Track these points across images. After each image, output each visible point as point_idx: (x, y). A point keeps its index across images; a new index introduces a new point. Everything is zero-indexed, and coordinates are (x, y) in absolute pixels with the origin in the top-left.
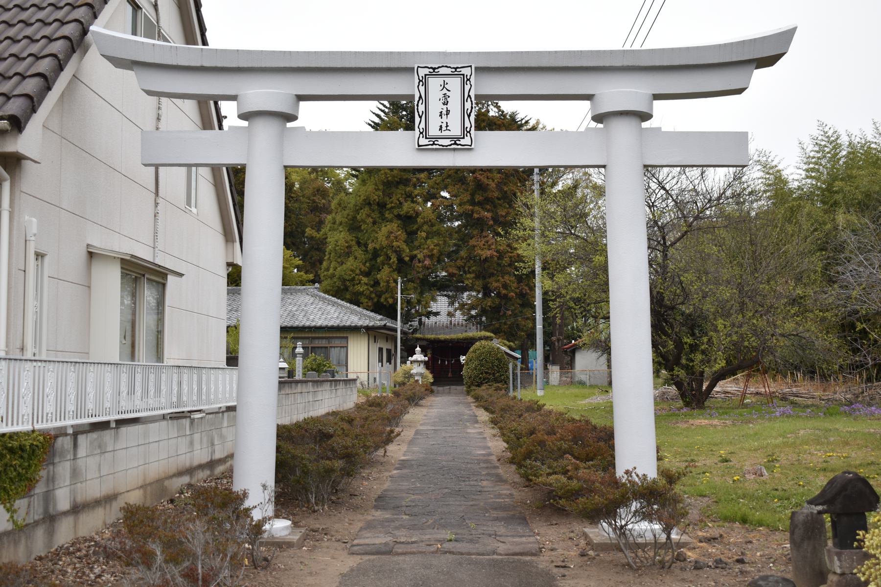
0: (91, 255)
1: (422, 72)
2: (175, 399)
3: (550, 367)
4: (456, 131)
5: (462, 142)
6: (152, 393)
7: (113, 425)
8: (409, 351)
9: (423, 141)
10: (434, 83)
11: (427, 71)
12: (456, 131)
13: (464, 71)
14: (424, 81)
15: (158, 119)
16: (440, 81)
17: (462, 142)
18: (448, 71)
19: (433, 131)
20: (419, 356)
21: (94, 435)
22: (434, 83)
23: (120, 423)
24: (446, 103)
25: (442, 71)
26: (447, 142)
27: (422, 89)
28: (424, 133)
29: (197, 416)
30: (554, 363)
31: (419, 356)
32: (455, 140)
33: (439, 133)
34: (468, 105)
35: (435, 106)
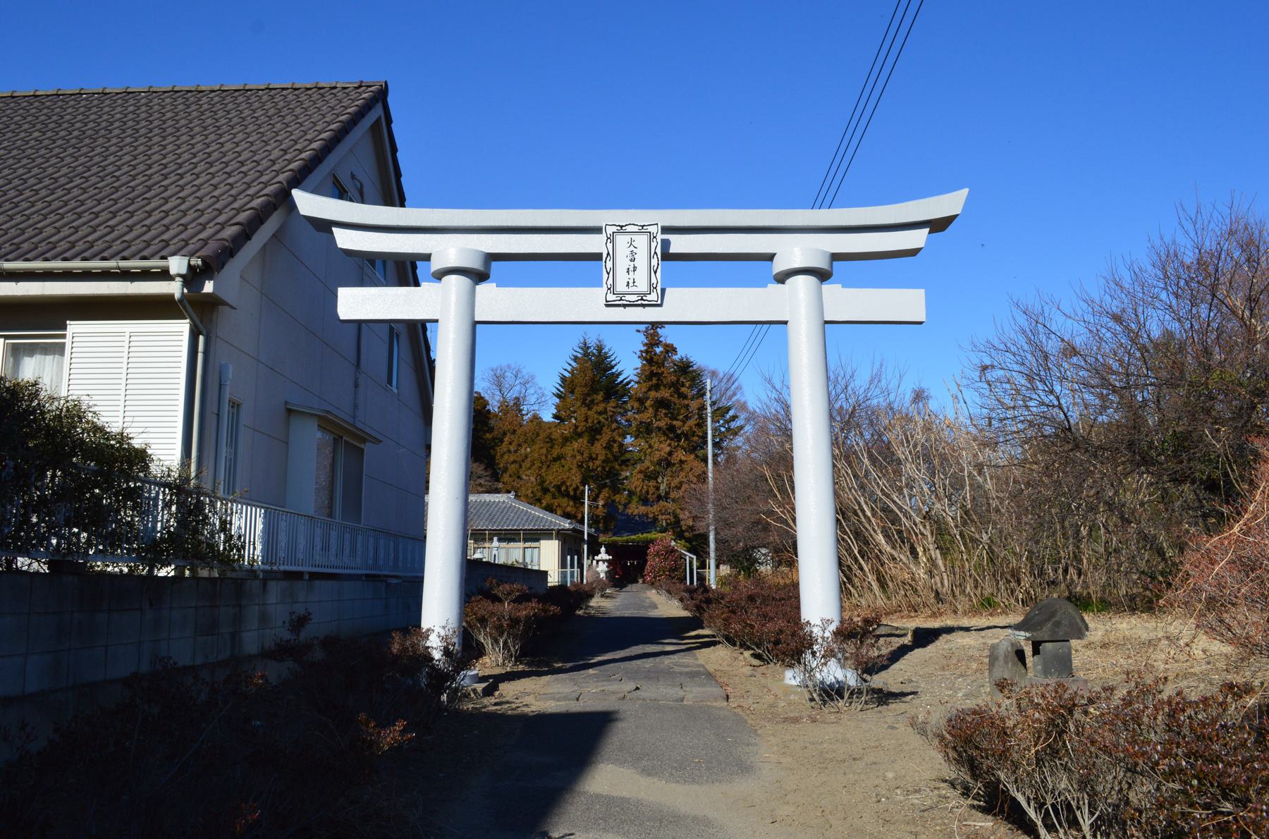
0: (290, 411)
1: (610, 230)
2: (371, 562)
3: (775, 407)
4: (643, 286)
5: (649, 298)
6: (347, 552)
7: (307, 577)
8: (594, 552)
9: (611, 297)
10: (622, 240)
11: (615, 229)
12: (643, 286)
13: (651, 229)
14: (611, 239)
15: (356, 386)
16: (627, 238)
17: (649, 298)
18: (636, 229)
19: (621, 287)
20: (603, 555)
21: (284, 584)
22: (622, 240)
23: (314, 576)
24: (633, 260)
25: (629, 228)
26: (634, 298)
27: (610, 246)
28: (612, 289)
29: (394, 581)
30: (724, 563)
31: (603, 555)
32: (642, 296)
33: (625, 289)
34: (654, 262)
35: (622, 262)
